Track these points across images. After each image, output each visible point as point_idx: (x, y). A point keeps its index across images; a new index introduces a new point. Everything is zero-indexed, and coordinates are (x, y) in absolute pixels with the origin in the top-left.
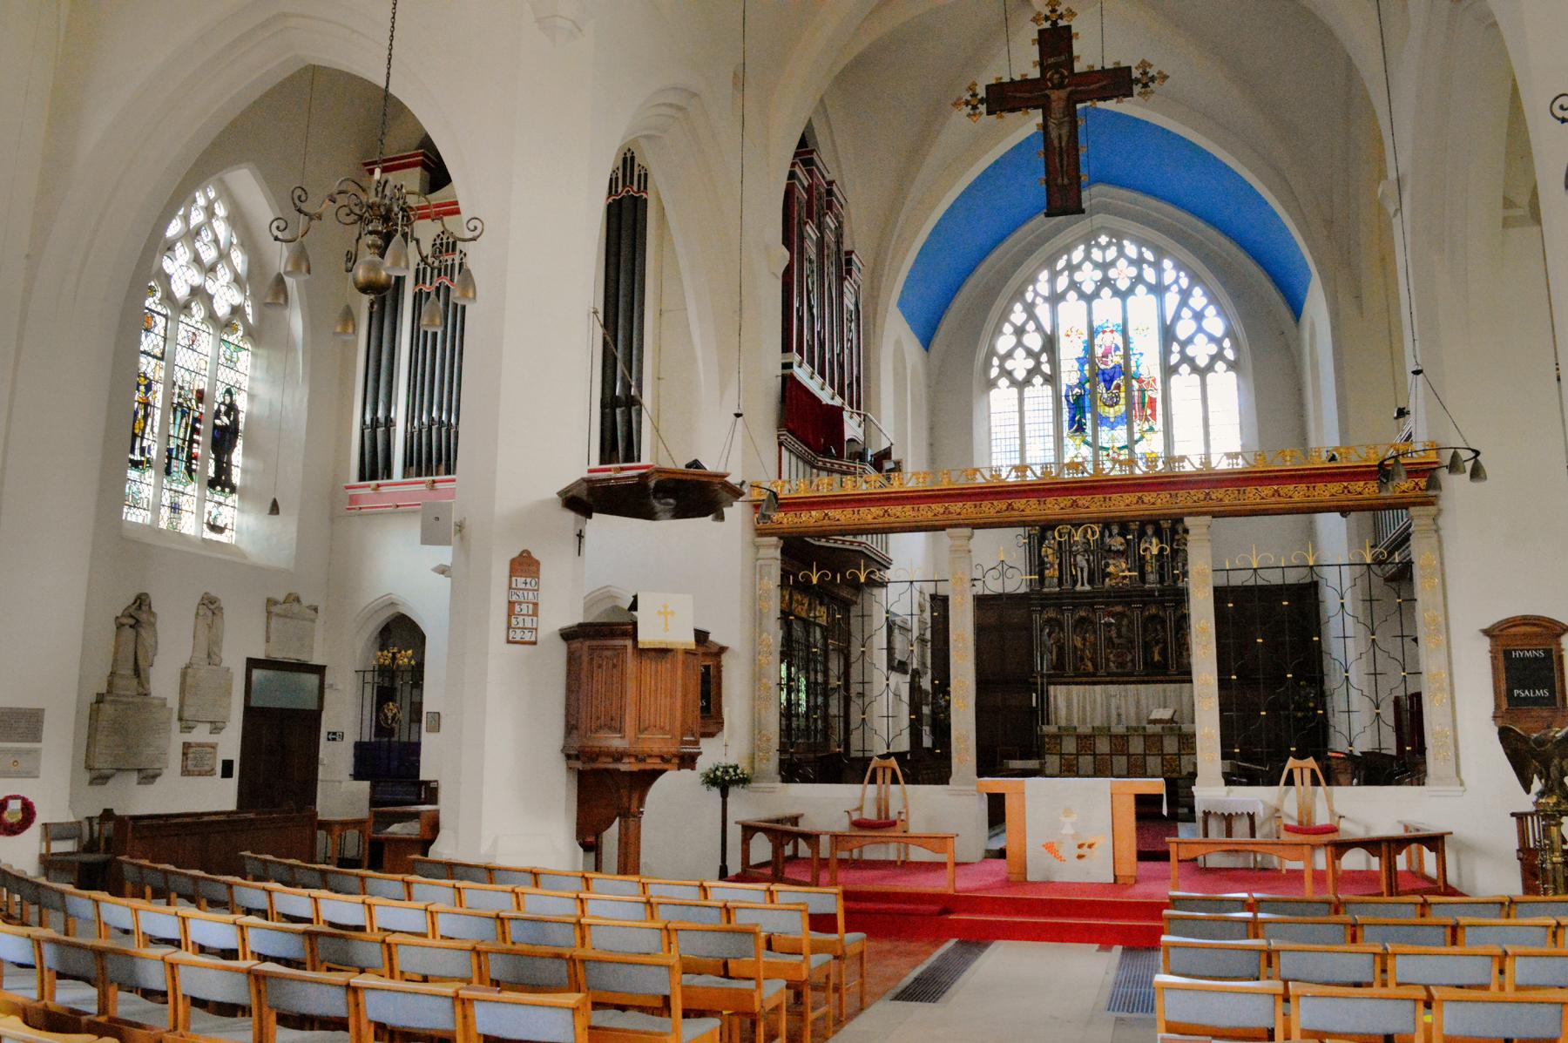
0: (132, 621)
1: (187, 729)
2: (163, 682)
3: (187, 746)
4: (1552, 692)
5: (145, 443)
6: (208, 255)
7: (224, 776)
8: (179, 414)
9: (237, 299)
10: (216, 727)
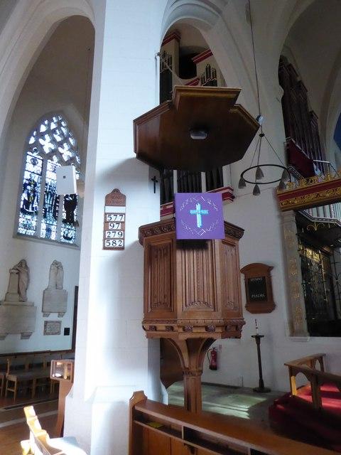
0: (17, 271)
1: (46, 314)
2: (35, 293)
3: (46, 323)
4: (266, 295)
5: (34, 206)
6: (59, 139)
7: (65, 334)
8: (49, 196)
9: (71, 155)
10: (61, 314)
